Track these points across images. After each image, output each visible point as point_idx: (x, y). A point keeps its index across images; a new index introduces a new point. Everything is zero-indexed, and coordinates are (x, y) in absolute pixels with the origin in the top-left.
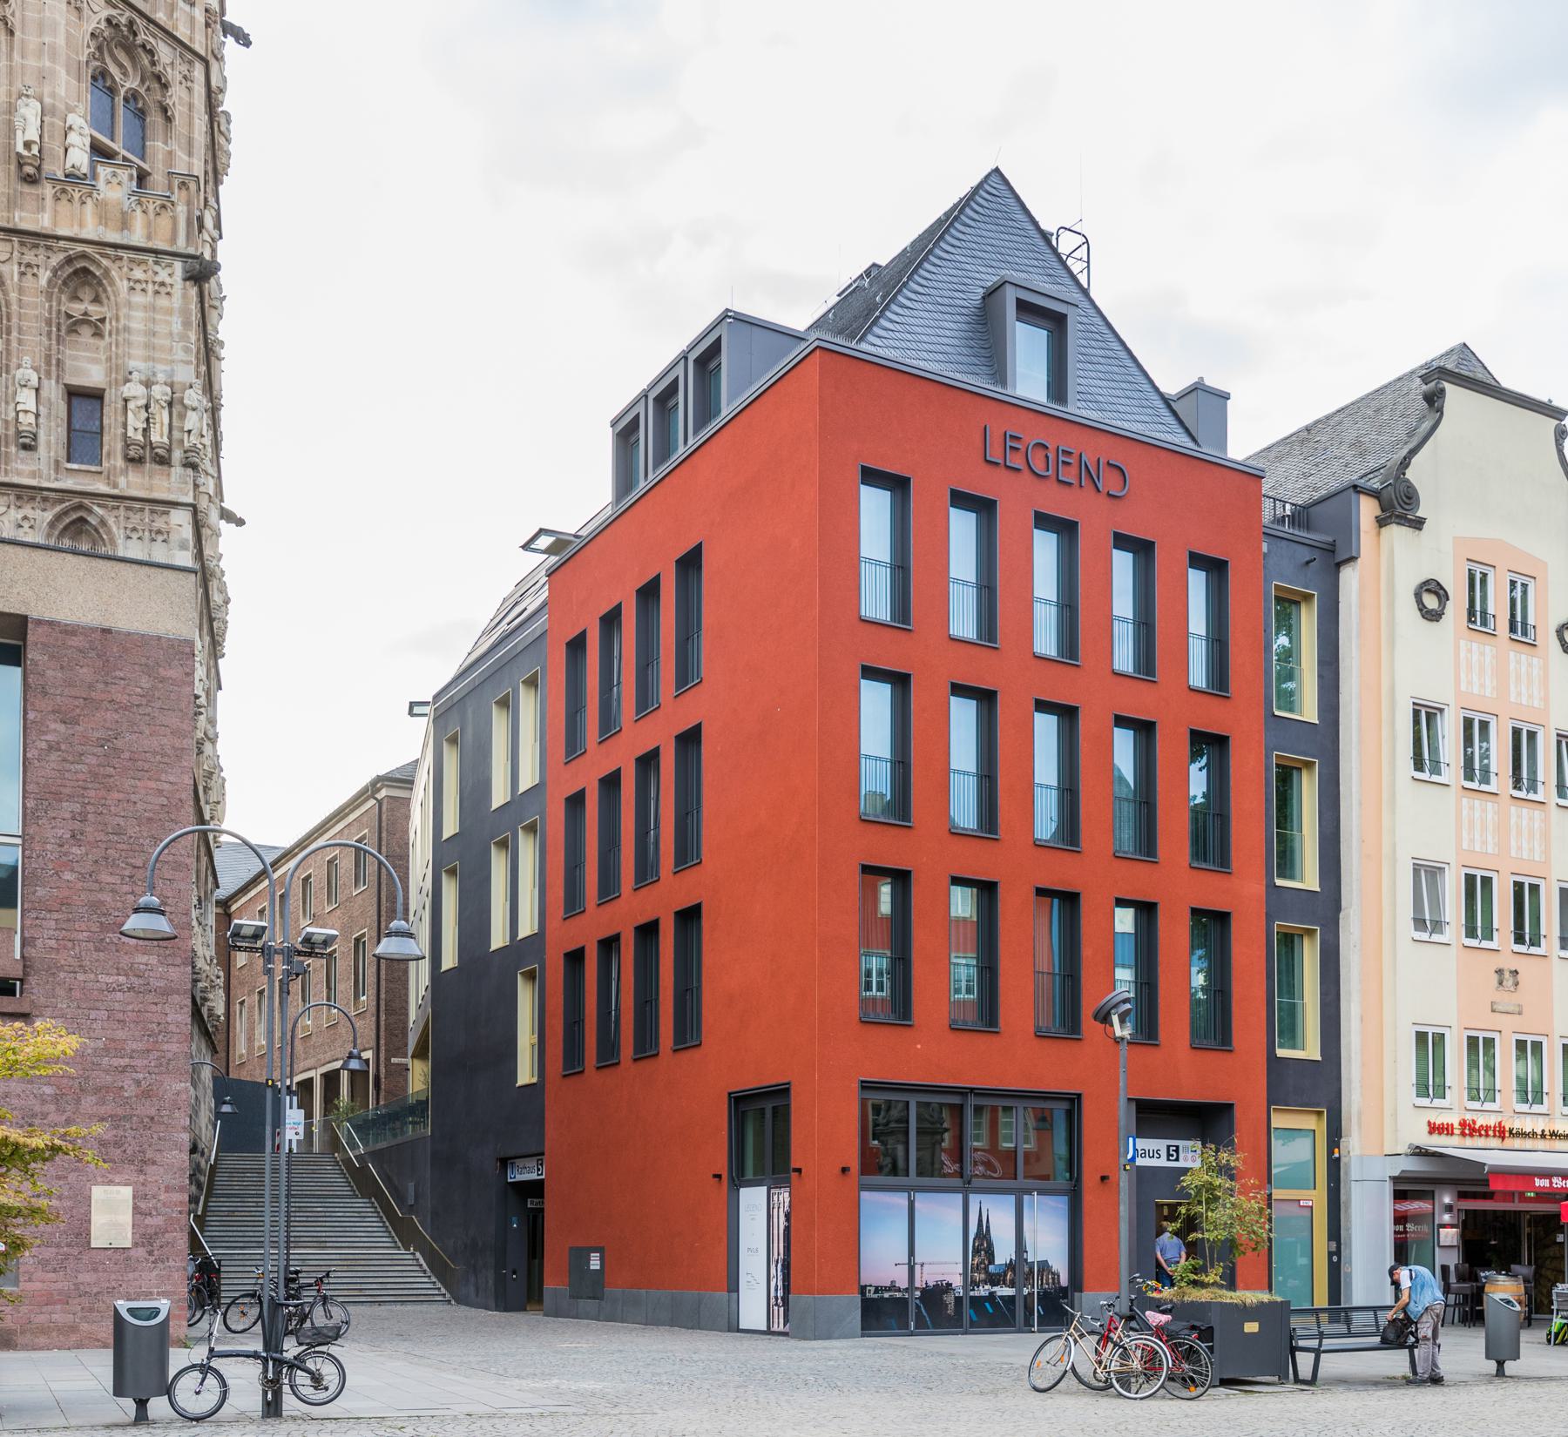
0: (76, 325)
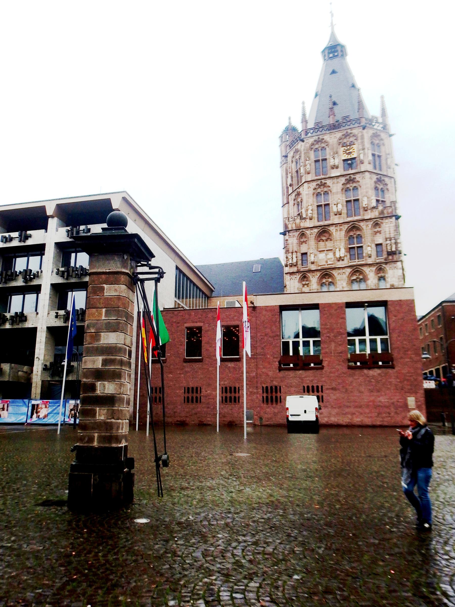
0: (376, 233)
